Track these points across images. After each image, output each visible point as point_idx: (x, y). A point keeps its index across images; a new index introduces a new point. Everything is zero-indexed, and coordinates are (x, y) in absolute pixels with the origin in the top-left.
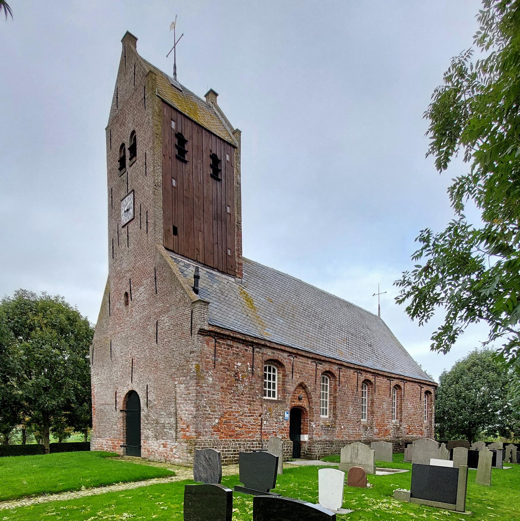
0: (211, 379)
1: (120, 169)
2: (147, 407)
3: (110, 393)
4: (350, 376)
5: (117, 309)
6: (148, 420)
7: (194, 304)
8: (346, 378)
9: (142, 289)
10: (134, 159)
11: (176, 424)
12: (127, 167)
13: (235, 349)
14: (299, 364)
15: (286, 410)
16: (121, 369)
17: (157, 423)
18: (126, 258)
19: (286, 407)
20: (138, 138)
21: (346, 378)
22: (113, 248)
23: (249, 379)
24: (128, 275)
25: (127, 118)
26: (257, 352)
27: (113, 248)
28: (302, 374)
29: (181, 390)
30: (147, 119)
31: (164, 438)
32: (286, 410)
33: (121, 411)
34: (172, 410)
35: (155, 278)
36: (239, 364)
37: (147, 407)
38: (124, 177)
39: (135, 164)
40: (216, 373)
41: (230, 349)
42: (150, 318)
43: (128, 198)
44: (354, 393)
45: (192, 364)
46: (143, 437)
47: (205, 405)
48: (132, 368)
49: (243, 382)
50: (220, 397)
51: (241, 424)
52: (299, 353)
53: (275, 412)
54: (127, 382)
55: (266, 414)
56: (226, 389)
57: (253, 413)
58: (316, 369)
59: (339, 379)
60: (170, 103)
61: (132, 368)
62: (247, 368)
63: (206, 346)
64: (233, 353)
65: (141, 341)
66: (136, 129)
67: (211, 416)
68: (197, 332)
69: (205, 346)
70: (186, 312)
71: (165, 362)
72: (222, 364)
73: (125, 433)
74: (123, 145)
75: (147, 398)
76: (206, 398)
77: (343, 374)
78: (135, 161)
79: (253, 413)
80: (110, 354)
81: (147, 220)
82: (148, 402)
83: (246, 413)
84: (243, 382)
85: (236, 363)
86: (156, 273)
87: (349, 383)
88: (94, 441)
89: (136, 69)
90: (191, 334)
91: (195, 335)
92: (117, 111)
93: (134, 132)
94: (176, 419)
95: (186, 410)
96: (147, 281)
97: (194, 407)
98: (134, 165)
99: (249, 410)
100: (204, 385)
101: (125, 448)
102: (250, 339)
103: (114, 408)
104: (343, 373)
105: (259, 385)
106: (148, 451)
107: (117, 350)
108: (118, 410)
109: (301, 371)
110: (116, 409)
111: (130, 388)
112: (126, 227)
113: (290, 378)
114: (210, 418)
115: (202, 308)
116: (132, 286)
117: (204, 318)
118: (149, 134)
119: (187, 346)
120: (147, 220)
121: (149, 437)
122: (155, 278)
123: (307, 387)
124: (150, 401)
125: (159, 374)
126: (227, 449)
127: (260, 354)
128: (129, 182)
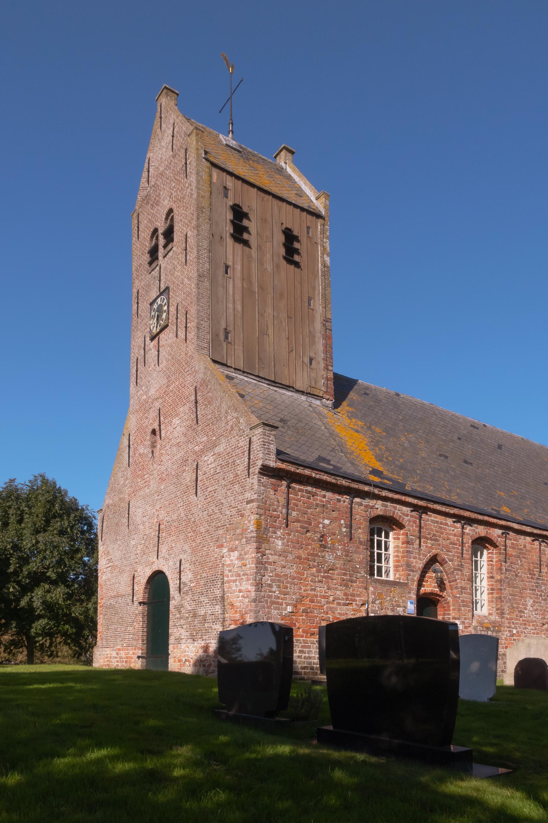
0: (280, 543)
1: (150, 263)
2: (180, 592)
3: (126, 578)
4: (525, 547)
5: (140, 454)
6: (180, 612)
7: (253, 430)
8: (518, 549)
9: (176, 421)
10: (170, 246)
11: (224, 614)
12: (160, 258)
13: (319, 498)
14: (430, 525)
15: (410, 598)
16: (143, 542)
17: (195, 616)
18: (155, 381)
19: (409, 593)
20: (177, 219)
21: (518, 549)
22: (137, 371)
23: (344, 545)
24: (158, 404)
25: (162, 195)
26: (357, 503)
27: (137, 371)
28: (436, 540)
29: (231, 560)
30: (189, 190)
31: (204, 637)
32: (410, 598)
33: (140, 603)
34: (218, 592)
35: (196, 402)
36: (327, 522)
37: (180, 592)
38: (155, 273)
39: (171, 252)
40: (289, 534)
41: (312, 498)
42: (188, 460)
43: (161, 298)
44: (535, 575)
45: (249, 519)
46: (172, 640)
47: (269, 582)
48: (159, 537)
49: (333, 549)
50: (295, 571)
51: (331, 617)
52: (431, 505)
53: (391, 600)
54: (151, 559)
55: (373, 602)
56: (305, 559)
57: (352, 600)
58: (463, 533)
59: (505, 550)
60: (223, 166)
61: (159, 537)
62: (341, 529)
63: (272, 492)
64: (317, 505)
65: (173, 496)
66: (174, 207)
67: (280, 601)
68: (257, 471)
69: (270, 492)
70: (241, 444)
71: (207, 521)
72: (298, 521)
73: (145, 638)
74: (156, 231)
75: (180, 579)
76: (272, 572)
77: (512, 544)
78: (171, 249)
79: (352, 600)
80: (127, 521)
81: (186, 324)
82: (182, 585)
83: (339, 599)
84: (333, 549)
85: (321, 521)
86: (198, 395)
87: (524, 558)
88: (98, 653)
89: (176, 130)
90: (249, 475)
91: (254, 475)
92: (149, 188)
93: (171, 211)
94: (224, 606)
95: (240, 591)
96: (185, 409)
97: (252, 584)
98: (170, 254)
99: (346, 594)
100: (267, 552)
101: (144, 660)
102: (344, 482)
103: (130, 601)
104: (512, 541)
105: (361, 556)
106: (180, 661)
107: (137, 513)
108: (136, 603)
109: (434, 535)
110: (133, 601)
111: (155, 568)
112: (157, 338)
113: (416, 546)
114: (278, 603)
115: (265, 435)
116: (162, 418)
117: (268, 449)
118: (192, 208)
119: (242, 492)
120: (186, 324)
121: (181, 639)
122: (196, 402)
123: (446, 562)
124: (185, 584)
125: (198, 541)
126: (307, 655)
127: (363, 507)
128: (162, 278)
